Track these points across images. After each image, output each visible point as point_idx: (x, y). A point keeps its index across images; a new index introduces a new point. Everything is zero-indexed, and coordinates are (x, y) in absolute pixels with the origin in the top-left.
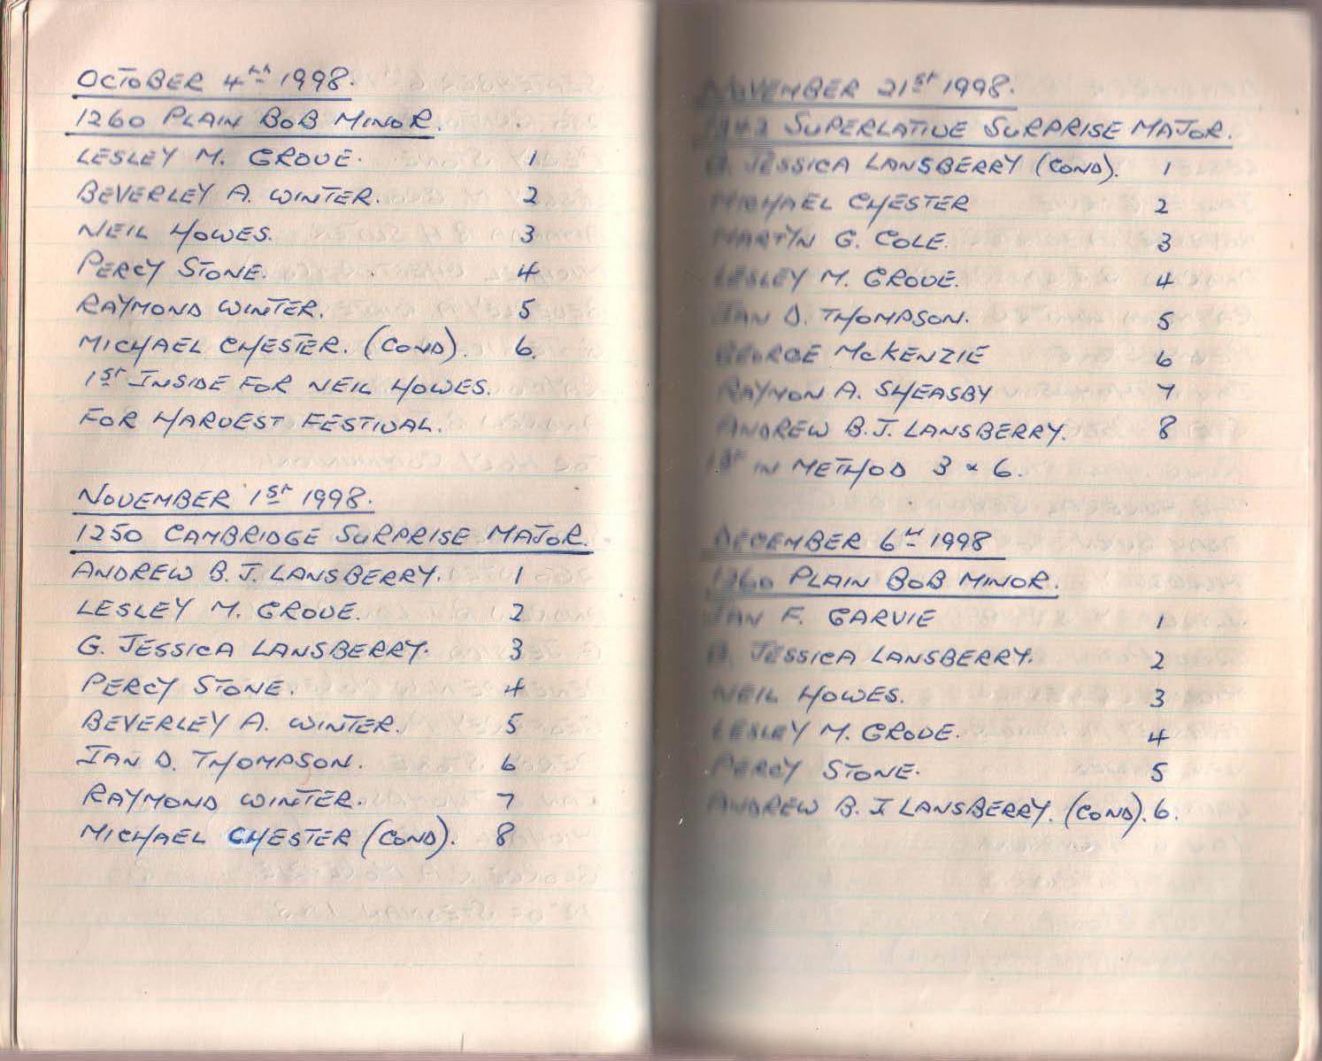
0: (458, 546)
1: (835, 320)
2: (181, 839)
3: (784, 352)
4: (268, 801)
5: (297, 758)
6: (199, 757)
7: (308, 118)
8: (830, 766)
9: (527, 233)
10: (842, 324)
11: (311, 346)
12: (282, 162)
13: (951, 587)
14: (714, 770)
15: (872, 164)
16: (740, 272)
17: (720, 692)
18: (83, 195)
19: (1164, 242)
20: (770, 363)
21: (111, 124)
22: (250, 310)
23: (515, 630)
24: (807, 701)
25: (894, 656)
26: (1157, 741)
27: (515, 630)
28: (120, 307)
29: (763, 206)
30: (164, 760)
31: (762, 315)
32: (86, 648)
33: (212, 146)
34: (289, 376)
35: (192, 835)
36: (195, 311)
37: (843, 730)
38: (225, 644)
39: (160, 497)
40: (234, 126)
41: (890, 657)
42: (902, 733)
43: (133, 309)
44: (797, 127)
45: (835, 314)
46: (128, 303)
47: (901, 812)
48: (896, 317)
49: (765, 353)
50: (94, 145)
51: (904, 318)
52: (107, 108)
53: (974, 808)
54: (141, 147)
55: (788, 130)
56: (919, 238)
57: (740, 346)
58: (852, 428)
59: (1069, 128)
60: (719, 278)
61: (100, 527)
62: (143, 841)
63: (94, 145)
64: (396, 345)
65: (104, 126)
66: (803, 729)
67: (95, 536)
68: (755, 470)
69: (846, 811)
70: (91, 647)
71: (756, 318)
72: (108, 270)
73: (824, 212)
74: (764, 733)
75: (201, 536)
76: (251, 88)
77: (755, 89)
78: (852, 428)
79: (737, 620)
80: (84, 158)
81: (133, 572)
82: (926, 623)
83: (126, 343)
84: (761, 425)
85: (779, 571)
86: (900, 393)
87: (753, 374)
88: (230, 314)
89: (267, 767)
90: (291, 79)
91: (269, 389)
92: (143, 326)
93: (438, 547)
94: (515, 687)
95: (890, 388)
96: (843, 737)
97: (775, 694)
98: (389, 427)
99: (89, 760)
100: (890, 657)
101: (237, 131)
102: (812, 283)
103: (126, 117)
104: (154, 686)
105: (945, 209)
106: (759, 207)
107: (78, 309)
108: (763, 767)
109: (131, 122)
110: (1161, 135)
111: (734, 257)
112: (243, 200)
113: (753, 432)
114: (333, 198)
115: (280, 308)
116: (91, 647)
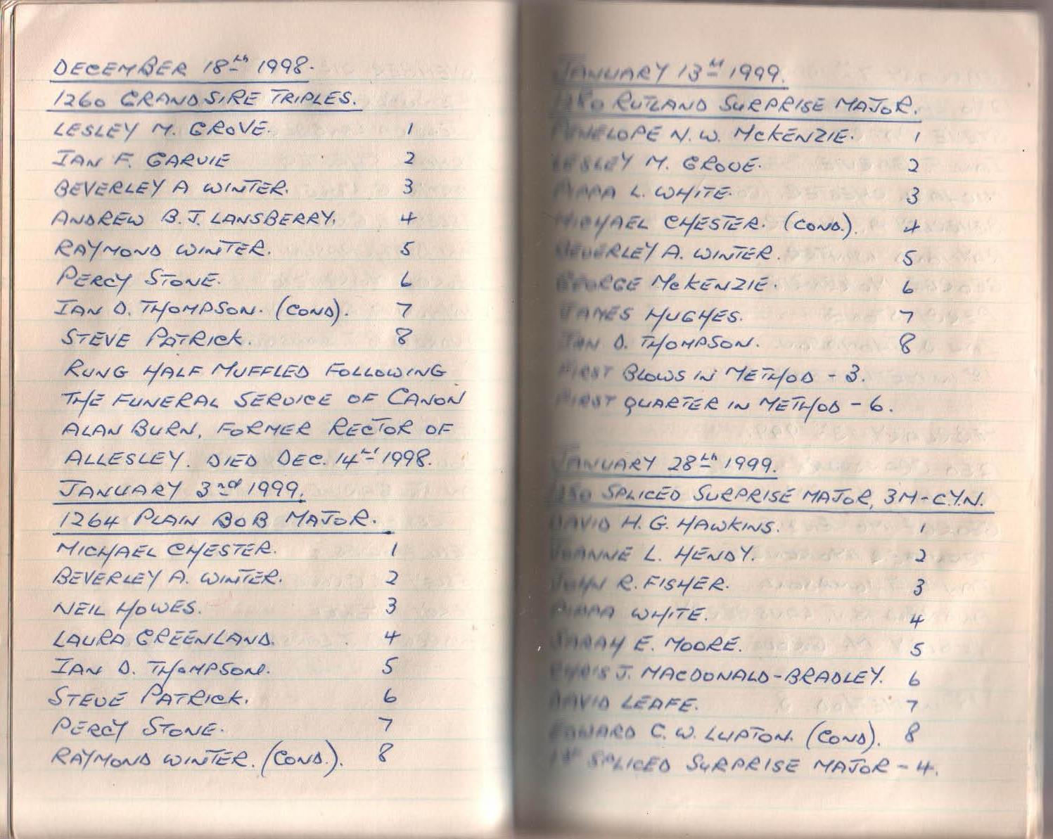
3: (614, 281)
4: (224, 187)
5: (216, 306)
7: (60, 189)
11: (253, 99)
12: (182, 405)
18: (58, 579)
19: (852, 373)
21: (81, 104)
23: (408, 171)
27: (408, 171)
30: (120, 309)
33: (165, 120)
34: (869, 491)
36: (155, 252)
40: (193, 524)
42: (714, 165)
44: (610, 494)
50: (69, 120)
52: (78, 91)
54: (107, 121)
55: (604, 496)
56: (694, 276)
63: (69, 120)
65: (76, 106)
66: (179, 458)
73: (627, 230)
74: (597, 165)
81: (99, 219)
83: (95, 549)
84: (600, 699)
87: (589, 239)
88: (187, 255)
89: (198, 673)
90: (733, 462)
94: (394, 639)
99: (59, 311)
101: (195, 528)
103: (92, 98)
104: (113, 281)
106: (593, 646)
107: (56, 253)
109: (96, 103)
111: (575, 235)
115: (229, 188)
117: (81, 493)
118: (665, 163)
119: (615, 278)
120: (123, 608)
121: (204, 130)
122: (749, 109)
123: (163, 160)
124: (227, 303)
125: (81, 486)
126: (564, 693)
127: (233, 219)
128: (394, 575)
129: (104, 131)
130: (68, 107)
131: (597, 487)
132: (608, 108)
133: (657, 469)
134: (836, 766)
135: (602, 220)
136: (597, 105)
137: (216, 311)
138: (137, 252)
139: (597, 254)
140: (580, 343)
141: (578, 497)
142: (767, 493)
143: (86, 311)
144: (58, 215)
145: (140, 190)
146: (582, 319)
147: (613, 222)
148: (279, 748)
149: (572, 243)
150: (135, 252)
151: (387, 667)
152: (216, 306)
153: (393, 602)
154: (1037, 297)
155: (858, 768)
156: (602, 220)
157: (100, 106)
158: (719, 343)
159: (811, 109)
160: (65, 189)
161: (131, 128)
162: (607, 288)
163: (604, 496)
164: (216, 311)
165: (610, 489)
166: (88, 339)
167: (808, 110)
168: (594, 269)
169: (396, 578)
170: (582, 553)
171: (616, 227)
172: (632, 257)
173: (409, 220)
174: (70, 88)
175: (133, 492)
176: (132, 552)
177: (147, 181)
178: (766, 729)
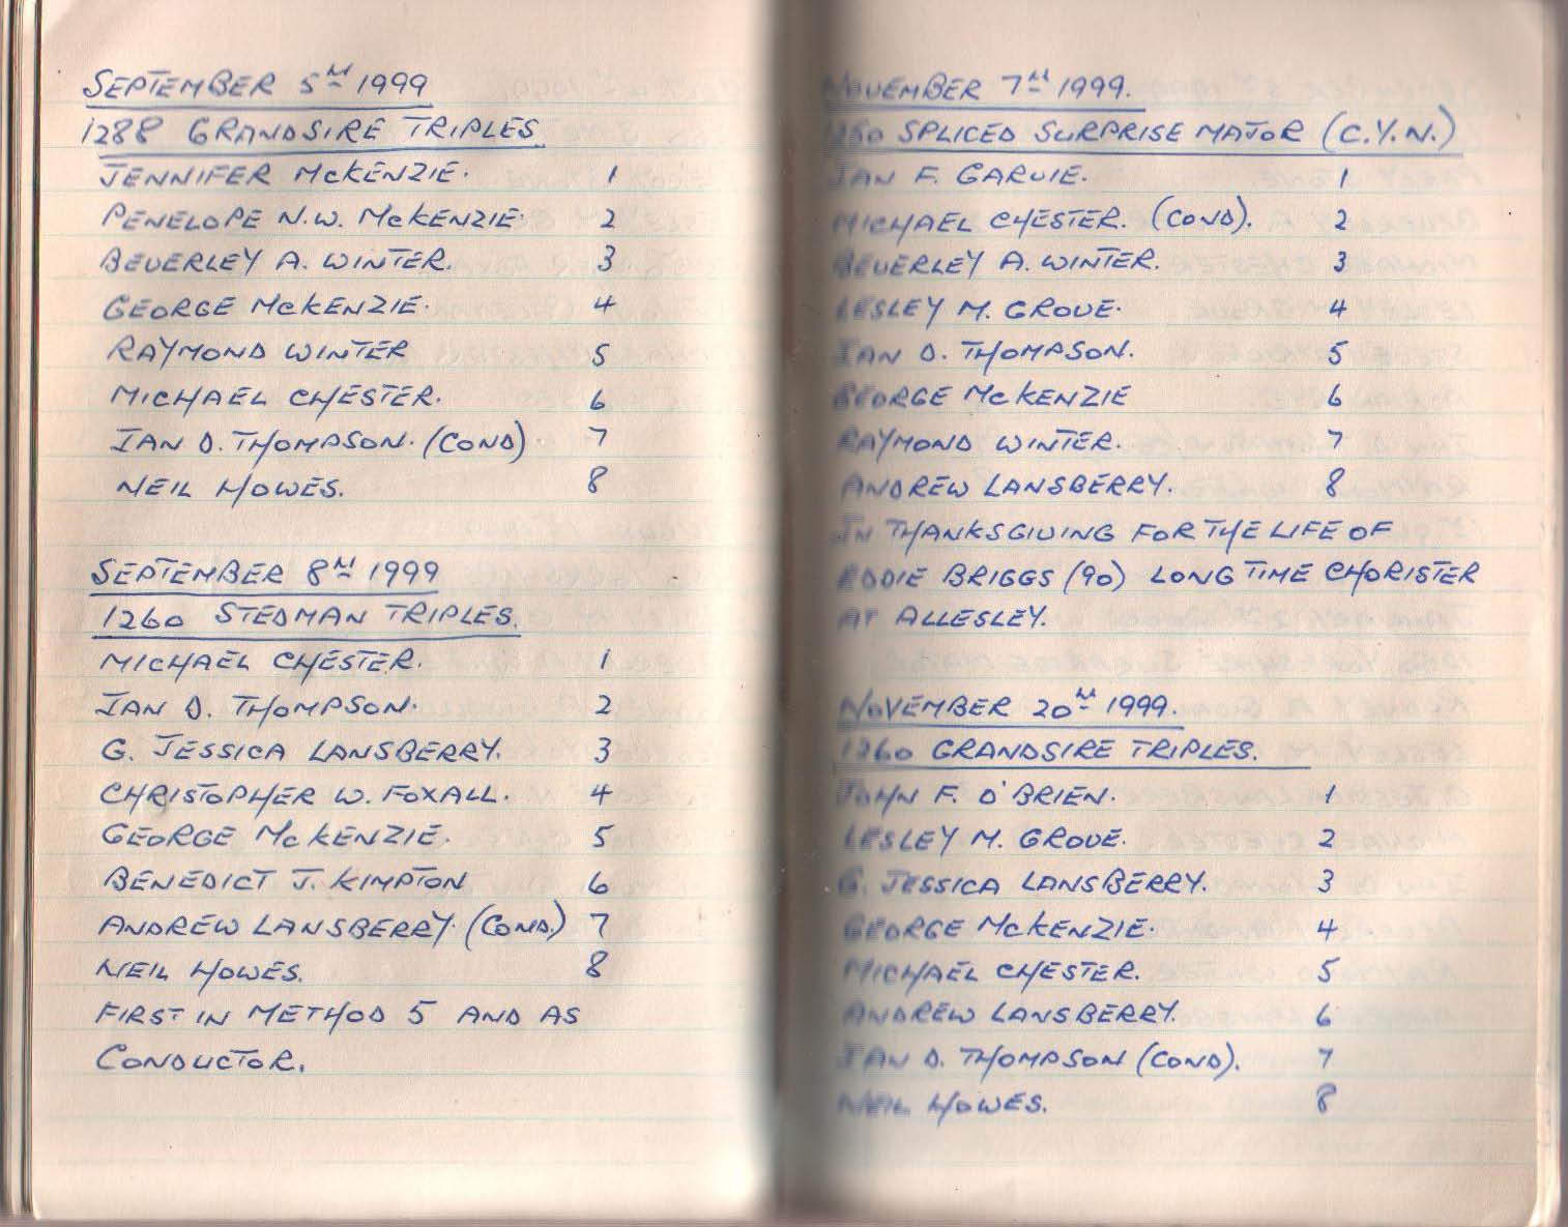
0: (112, 99)
2: (239, 400)
5: (347, 702)
10: (983, 1065)
15: (990, 491)
16: (869, 965)
17: (844, 1102)
24: (201, 978)
25: (114, 921)
26: (603, 308)
28: (161, 352)
29: (903, 976)
31: (899, 1057)
32: (110, 752)
35: (251, 395)
37: (982, 308)
39: (188, 82)
41: (1013, 1016)
45: (976, 1055)
46: (172, 348)
48: (1041, 1058)
49: (902, 929)
53: (227, 574)
55: (902, 139)
57: (860, 387)
58: (931, 87)
60: (848, 840)
61: (128, 612)
64: (1182, 217)
70: (115, 752)
71: (886, 355)
72: (144, 308)
75: (997, 751)
76: (322, 93)
78: (931, 87)
82: (380, 933)
85: (922, 743)
87: (871, 287)
91: (140, 1064)
92: (186, 376)
94: (605, 302)
97: (904, 1104)
100: (1013, 1016)
108: (851, 438)
110: (1228, 138)
114: (366, 664)
116: (115, 752)
118: (986, 311)
120: (177, 662)
122: (969, 582)
124: (364, 697)
128: (611, 251)
129: (217, 263)
130: (125, 632)
131: (892, 124)
134: (1228, 134)
135: (902, 222)
137: (346, 708)
139: (895, 269)
140: (867, 355)
141: (865, 137)
146: (865, 364)
148: (1218, 1071)
149: (858, 258)
151: (597, 356)
152: (347, 702)
155: (1259, 134)
156: (902, 222)
158: (1083, 351)
159: (1163, 137)
160: (112, 263)
163: (902, 139)
164: (346, 708)
165: (907, 127)
170: (857, 485)
171: (923, 230)
173: (1329, 930)
176: (945, 973)
177: (259, 209)
178: (1205, 1054)
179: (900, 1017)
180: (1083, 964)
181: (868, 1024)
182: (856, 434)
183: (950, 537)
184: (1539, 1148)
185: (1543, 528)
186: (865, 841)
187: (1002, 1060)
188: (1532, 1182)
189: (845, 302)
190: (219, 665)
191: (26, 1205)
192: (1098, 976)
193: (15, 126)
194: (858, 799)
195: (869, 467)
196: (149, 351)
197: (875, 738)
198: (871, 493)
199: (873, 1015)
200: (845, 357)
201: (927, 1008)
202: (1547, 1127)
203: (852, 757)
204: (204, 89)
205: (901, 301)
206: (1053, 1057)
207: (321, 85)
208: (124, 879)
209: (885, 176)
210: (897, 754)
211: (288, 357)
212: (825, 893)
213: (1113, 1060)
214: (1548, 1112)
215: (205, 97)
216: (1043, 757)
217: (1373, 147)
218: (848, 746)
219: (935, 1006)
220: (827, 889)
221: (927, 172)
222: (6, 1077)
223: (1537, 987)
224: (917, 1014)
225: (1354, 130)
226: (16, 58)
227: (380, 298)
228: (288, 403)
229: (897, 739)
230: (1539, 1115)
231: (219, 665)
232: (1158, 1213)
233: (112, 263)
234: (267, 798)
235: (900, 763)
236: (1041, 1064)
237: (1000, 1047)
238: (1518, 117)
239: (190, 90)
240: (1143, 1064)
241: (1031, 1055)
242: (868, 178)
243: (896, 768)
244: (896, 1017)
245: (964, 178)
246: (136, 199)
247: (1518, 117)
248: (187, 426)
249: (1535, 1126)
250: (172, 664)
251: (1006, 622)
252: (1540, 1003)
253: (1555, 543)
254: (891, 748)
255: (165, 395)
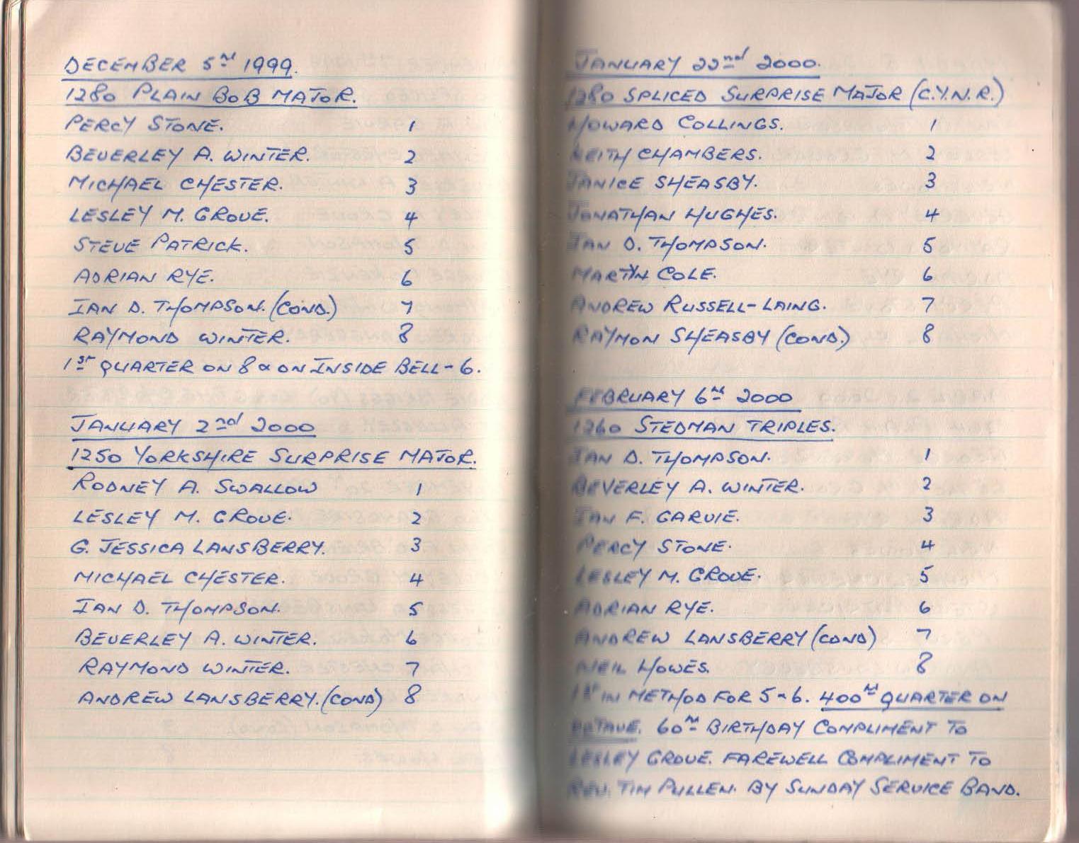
1: (669, 700)
6: (166, 606)
8: (646, 429)
9: (411, 186)
13: (266, 98)
14: (580, 547)
17: (577, 271)
20: (608, 282)
22: (260, 639)
26: (416, 582)
30: (140, 608)
37: (193, 515)
38: (189, 481)
43: (120, 338)
47: (195, 551)
51: (772, 94)
59: (784, 94)
60: (579, 579)
62: (693, 341)
67: (76, 310)
68: (603, 699)
69: (85, 641)
76: (216, 69)
77: (597, 518)
79: (593, 459)
80: (200, 549)
84: (609, 635)
85: (629, 421)
86: (692, 338)
91: (684, 277)
93: (799, 101)
95: (797, 785)
96: (675, 581)
98: (244, 639)
102: (651, 551)
105: (120, 554)
108: (583, 332)
112: (193, 492)
113: (603, 641)
117: (91, 427)
119: (621, 545)
121: (226, 518)
123: (702, 576)
125: (89, 421)
126: (585, 718)
127: (214, 547)
132: (618, 100)
133: (681, 69)
136: (607, 97)
138: (164, 670)
140: (596, 518)
142: (799, 92)
143: (107, 608)
144: (85, 695)
145: (166, 641)
147: (673, 155)
150: (162, 669)
153: (412, 183)
154: (1053, 135)
157: (110, 100)
160: (77, 154)
161: (145, 210)
162: (619, 493)
166: (98, 246)
167: (794, 790)
168: (604, 594)
169: (413, 158)
170: (587, 183)
172: (123, 219)
174: (77, 85)
175: (139, 428)
179: (614, 640)
180: (242, 179)
181: (592, 645)
182: (581, 783)
183: (648, 612)
184: (1052, 787)
185: (1059, 772)
186: (590, 490)
187: (685, 460)
188: (1047, 807)
189: (583, 570)
190: (150, 581)
191: (19, 831)
192: (170, 369)
193: (7, 92)
194: (583, 216)
195: (591, 140)
196: (108, 667)
197: (596, 418)
198: (596, 643)
199: (596, 639)
200: (576, 245)
201: (633, 633)
202: (1056, 773)
203: (581, 431)
204: (139, 68)
205: (622, 573)
206: (719, 457)
207: (216, 64)
208: (79, 153)
209: (609, 517)
210: (611, 429)
211: (204, 671)
212: (564, 614)
213: (758, 459)
214: (1057, 763)
215: (140, 72)
216: (707, 309)
217: (938, 102)
218: (578, 424)
219: (639, 633)
220: (566, 612)
221: (635, 515)
222: (5, 606)
223: (1049, 678)
224: (626, 638)
225: (926, 92)
226: (7, 46)
227: (82, 669)
228: (194, 219)
229: (611, 419)
230: (1052, 766)
231: (150, 581)
232: (790, 834)
233: (77, 154)
234: (178, 309)
235: (612, 435)
236: (711, 461)
237: (677, 238)
238: (1039, 84)
239: (130, 69)
240: (780, 343)
241: (703, 457)
242: (599, 518)
243: (610, 438)
244: (611, 640)
245: (662, 519)
246: (91, 140)
247: (1039, 84)
248: (124, 294)
249: (1049, 774)
250: (120, 578)
251: (80, 219)
252: (1052, 695)
253: (1061, 375)
254: (607, 426)
255: (111, 576)
